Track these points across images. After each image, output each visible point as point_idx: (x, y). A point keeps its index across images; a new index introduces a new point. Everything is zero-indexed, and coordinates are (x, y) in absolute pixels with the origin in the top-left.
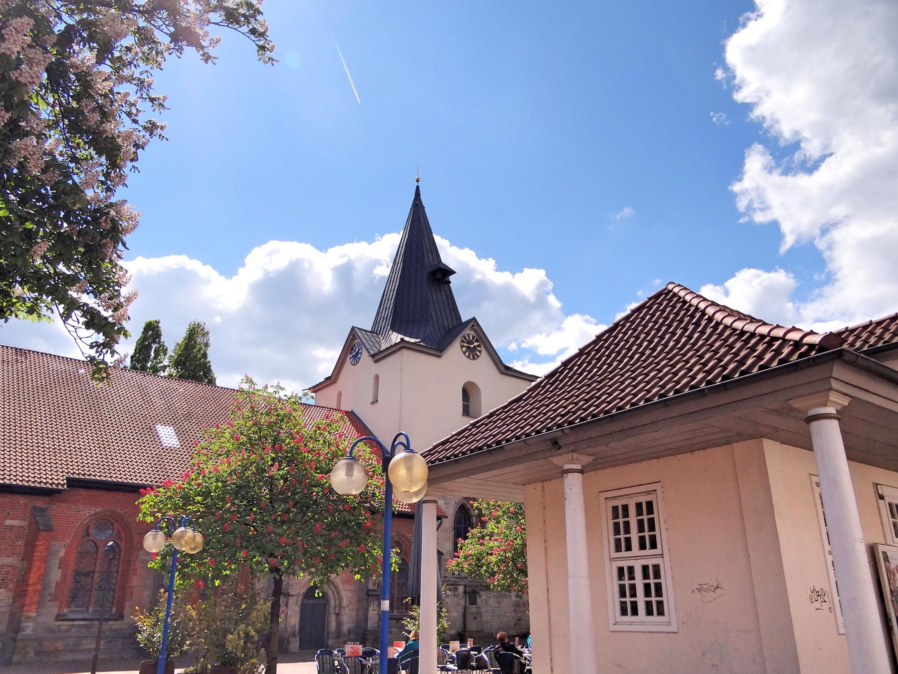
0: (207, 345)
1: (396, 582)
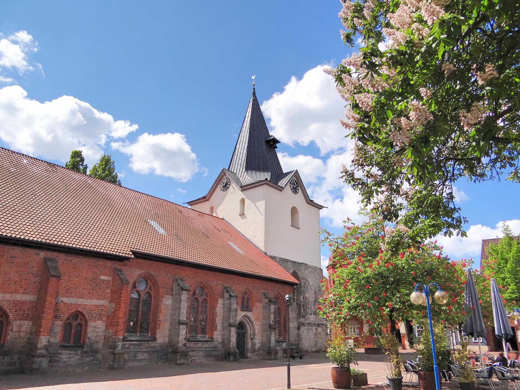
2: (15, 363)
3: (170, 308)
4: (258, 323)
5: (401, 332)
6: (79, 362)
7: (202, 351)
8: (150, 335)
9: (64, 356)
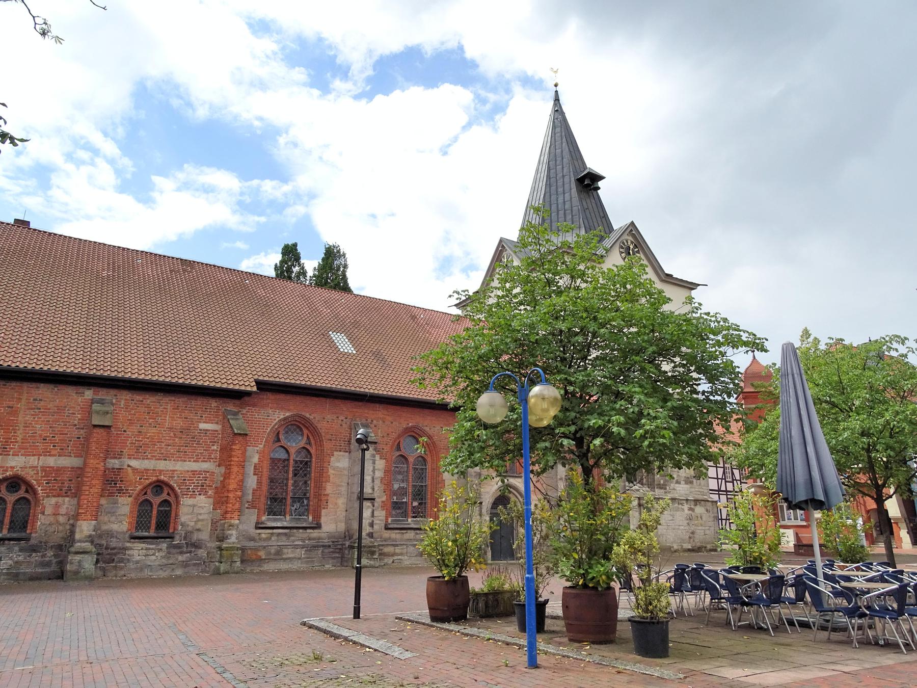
0: (345, 266)
2: (48, 564)
3: (346, 472)
5: (890, 515)
9: (135, 553)
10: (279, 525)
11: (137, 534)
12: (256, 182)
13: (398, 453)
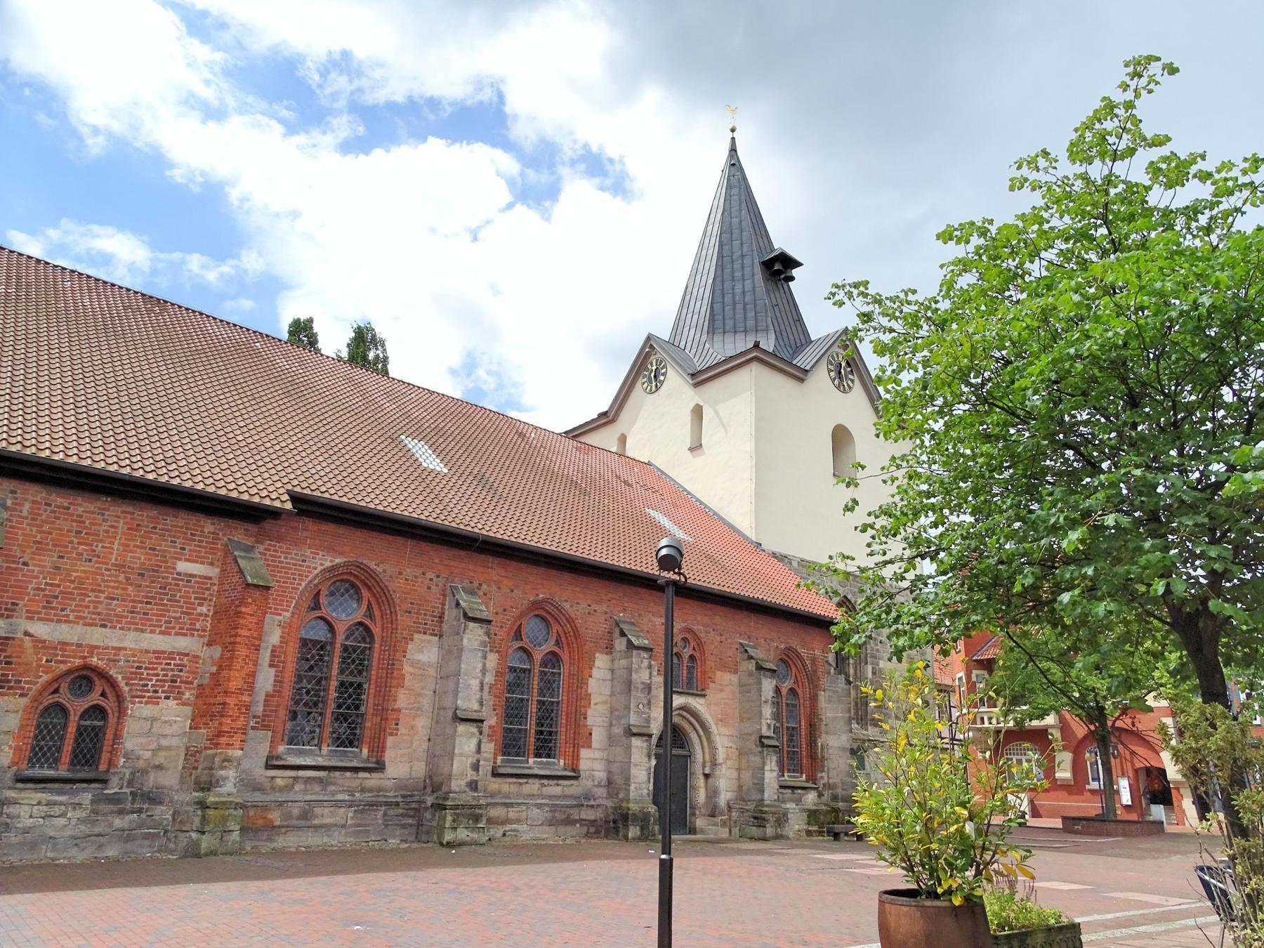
1: (785, 725)
3: (432, 672)
4: (724, 730)
6: (85, 829)
7: (539, 806)
8: (365, 751)
9: (24, 811)
10: (309, 761)
11: (30, 773)
12: (177, 256)
13: (518, 644)
